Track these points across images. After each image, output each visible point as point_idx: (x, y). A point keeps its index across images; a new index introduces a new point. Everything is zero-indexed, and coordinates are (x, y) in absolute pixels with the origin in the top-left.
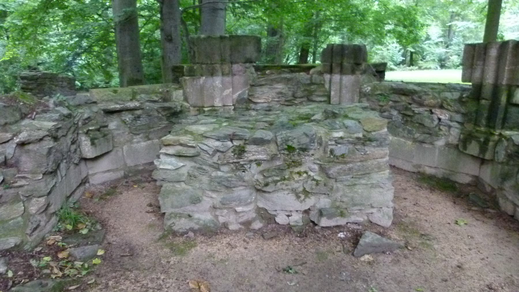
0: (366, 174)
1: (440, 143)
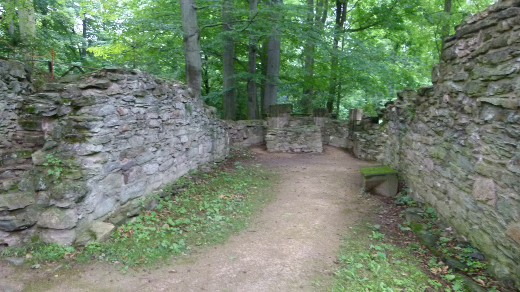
0: (315, 140)
1: (345, 137)
